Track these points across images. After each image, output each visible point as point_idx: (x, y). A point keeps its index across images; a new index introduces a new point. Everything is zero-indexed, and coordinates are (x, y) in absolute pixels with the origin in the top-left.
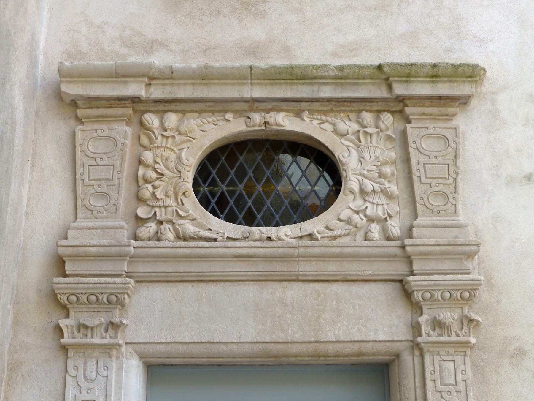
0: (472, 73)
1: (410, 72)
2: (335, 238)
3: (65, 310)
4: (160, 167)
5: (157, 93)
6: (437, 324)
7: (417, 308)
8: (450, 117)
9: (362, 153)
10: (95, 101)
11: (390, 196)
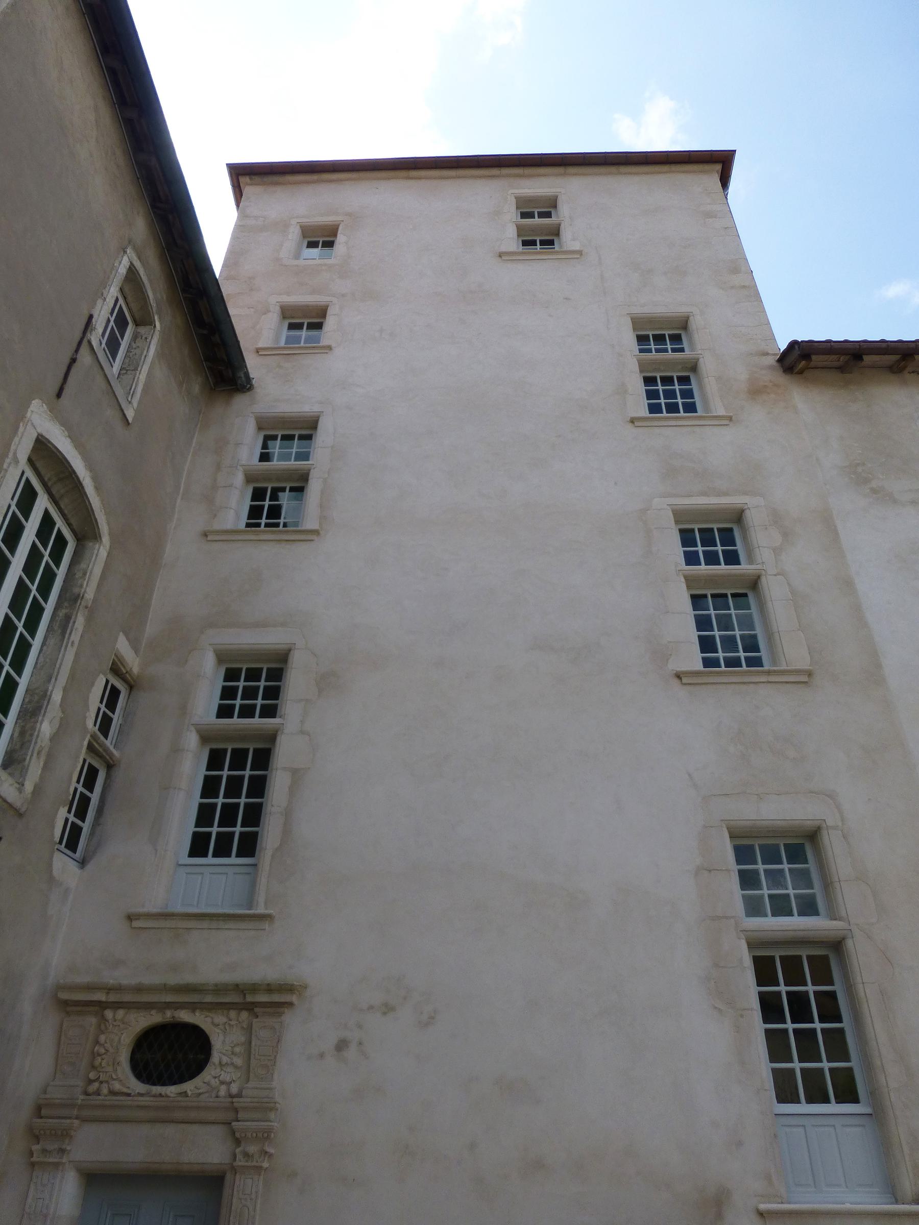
0: (289, 988)
1: (254, 988)
2: (200, 1094)
3: (37, 1139)
4: (108, 1045)
5: (112, 998)
6: (246, 1155)
7: (238, 1142)
8: (280, 1014)
9: (224, 1039)
10: (78, 1004)
11: (236, 1067)
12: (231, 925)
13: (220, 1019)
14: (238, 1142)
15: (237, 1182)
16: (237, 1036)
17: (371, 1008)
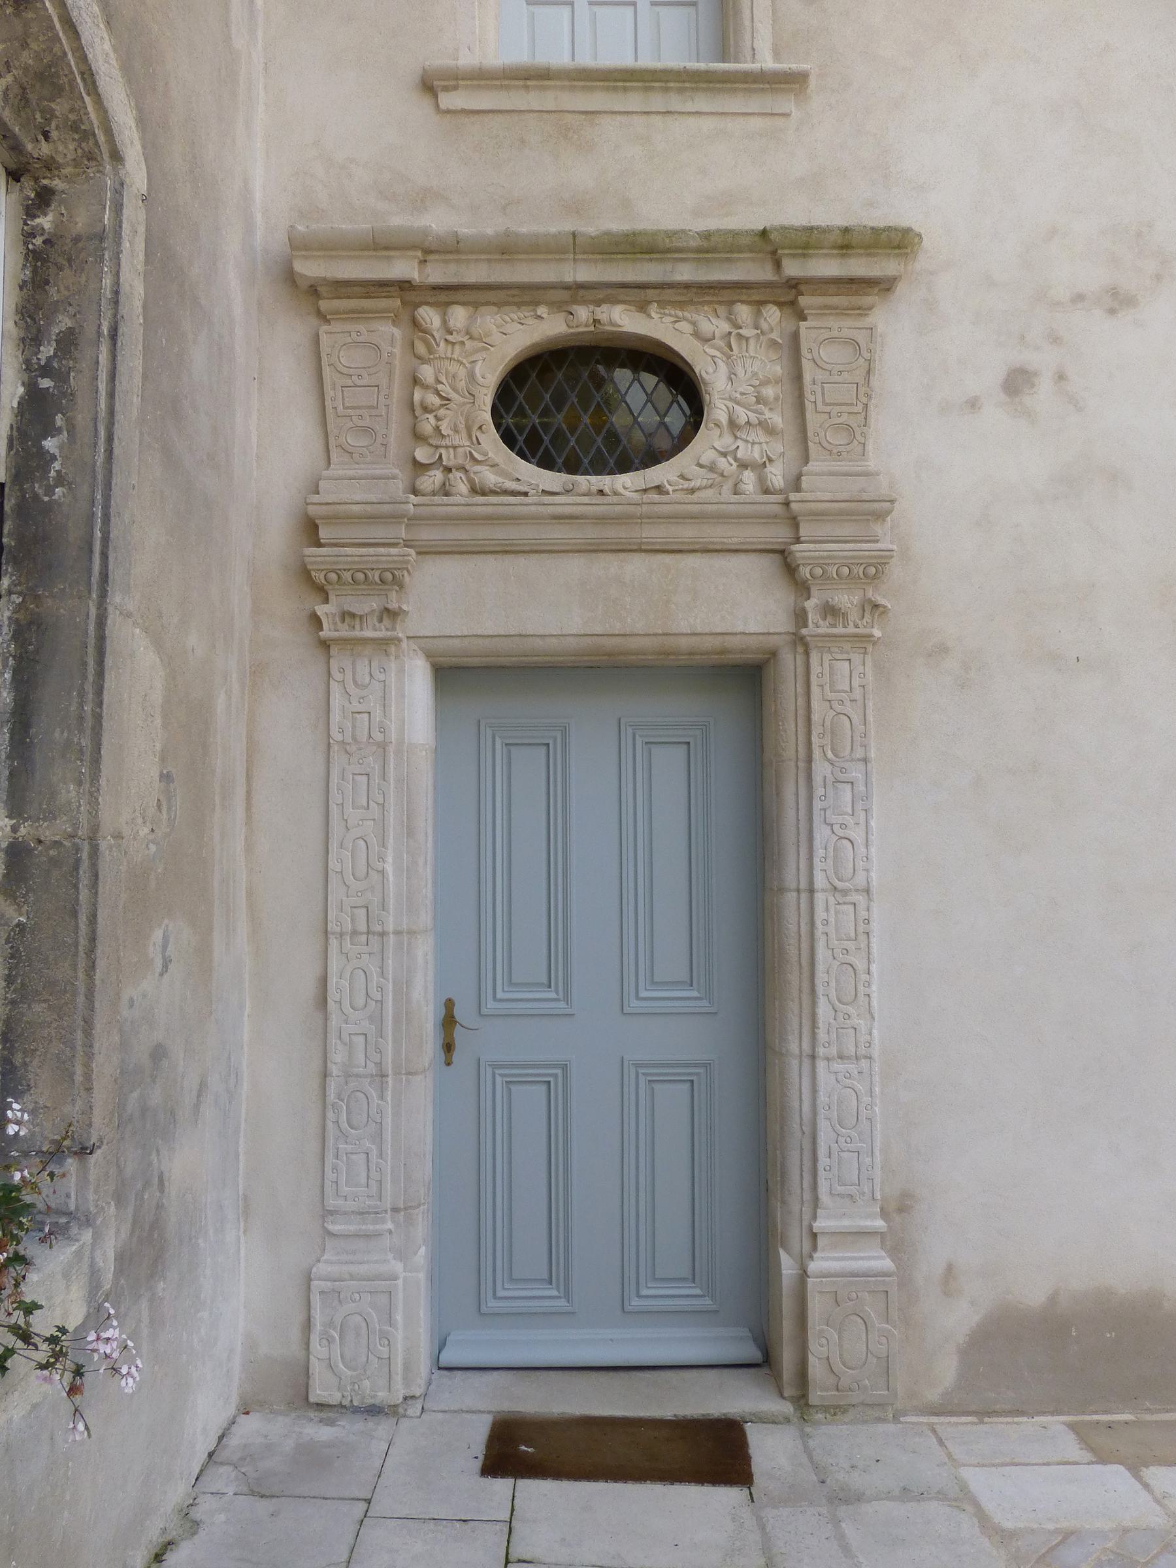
0: (898, 242)
1: (808, 240)
2: (692, 491)
4: (445, 389)
5: (437, 274)
6: (830, 611)
8: (863, 311)
9: (732, 364)
10: (344, 287)
11: (771, 431)
12: (702, 103)
13: (714, 324)
14: (802, 588)
15: (815, 669)
16: (761, 364)
17: (1079, 298)
